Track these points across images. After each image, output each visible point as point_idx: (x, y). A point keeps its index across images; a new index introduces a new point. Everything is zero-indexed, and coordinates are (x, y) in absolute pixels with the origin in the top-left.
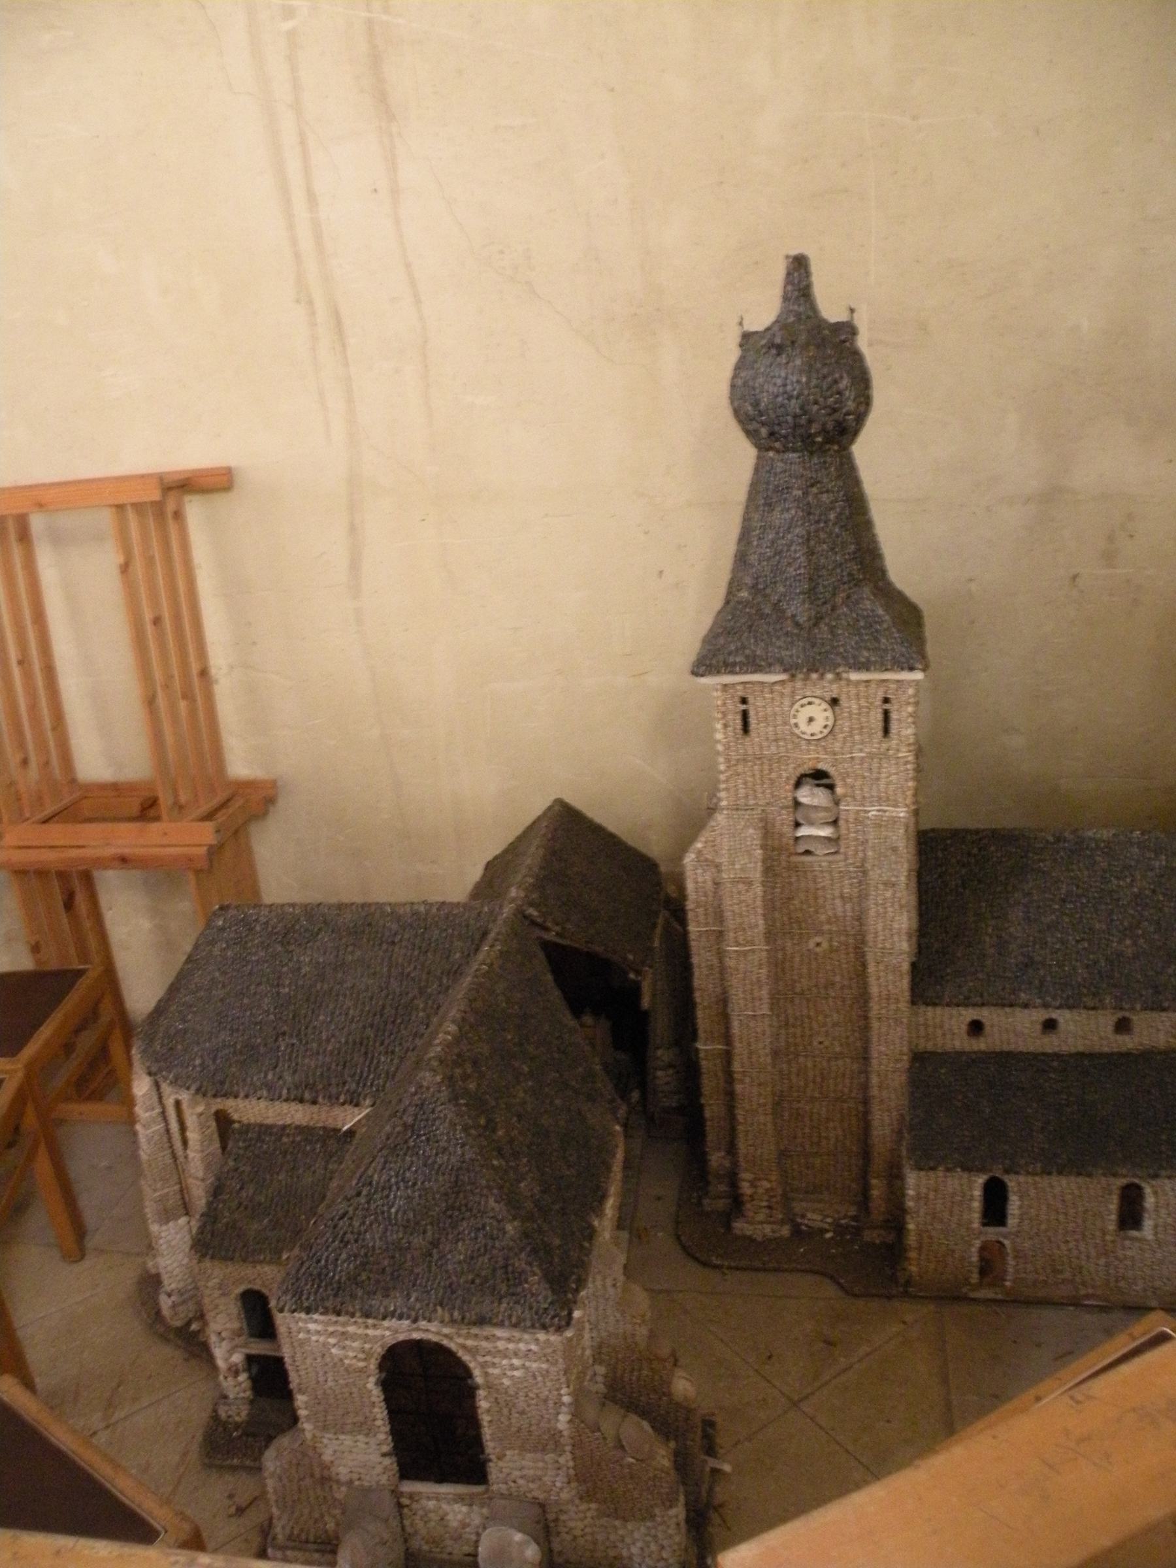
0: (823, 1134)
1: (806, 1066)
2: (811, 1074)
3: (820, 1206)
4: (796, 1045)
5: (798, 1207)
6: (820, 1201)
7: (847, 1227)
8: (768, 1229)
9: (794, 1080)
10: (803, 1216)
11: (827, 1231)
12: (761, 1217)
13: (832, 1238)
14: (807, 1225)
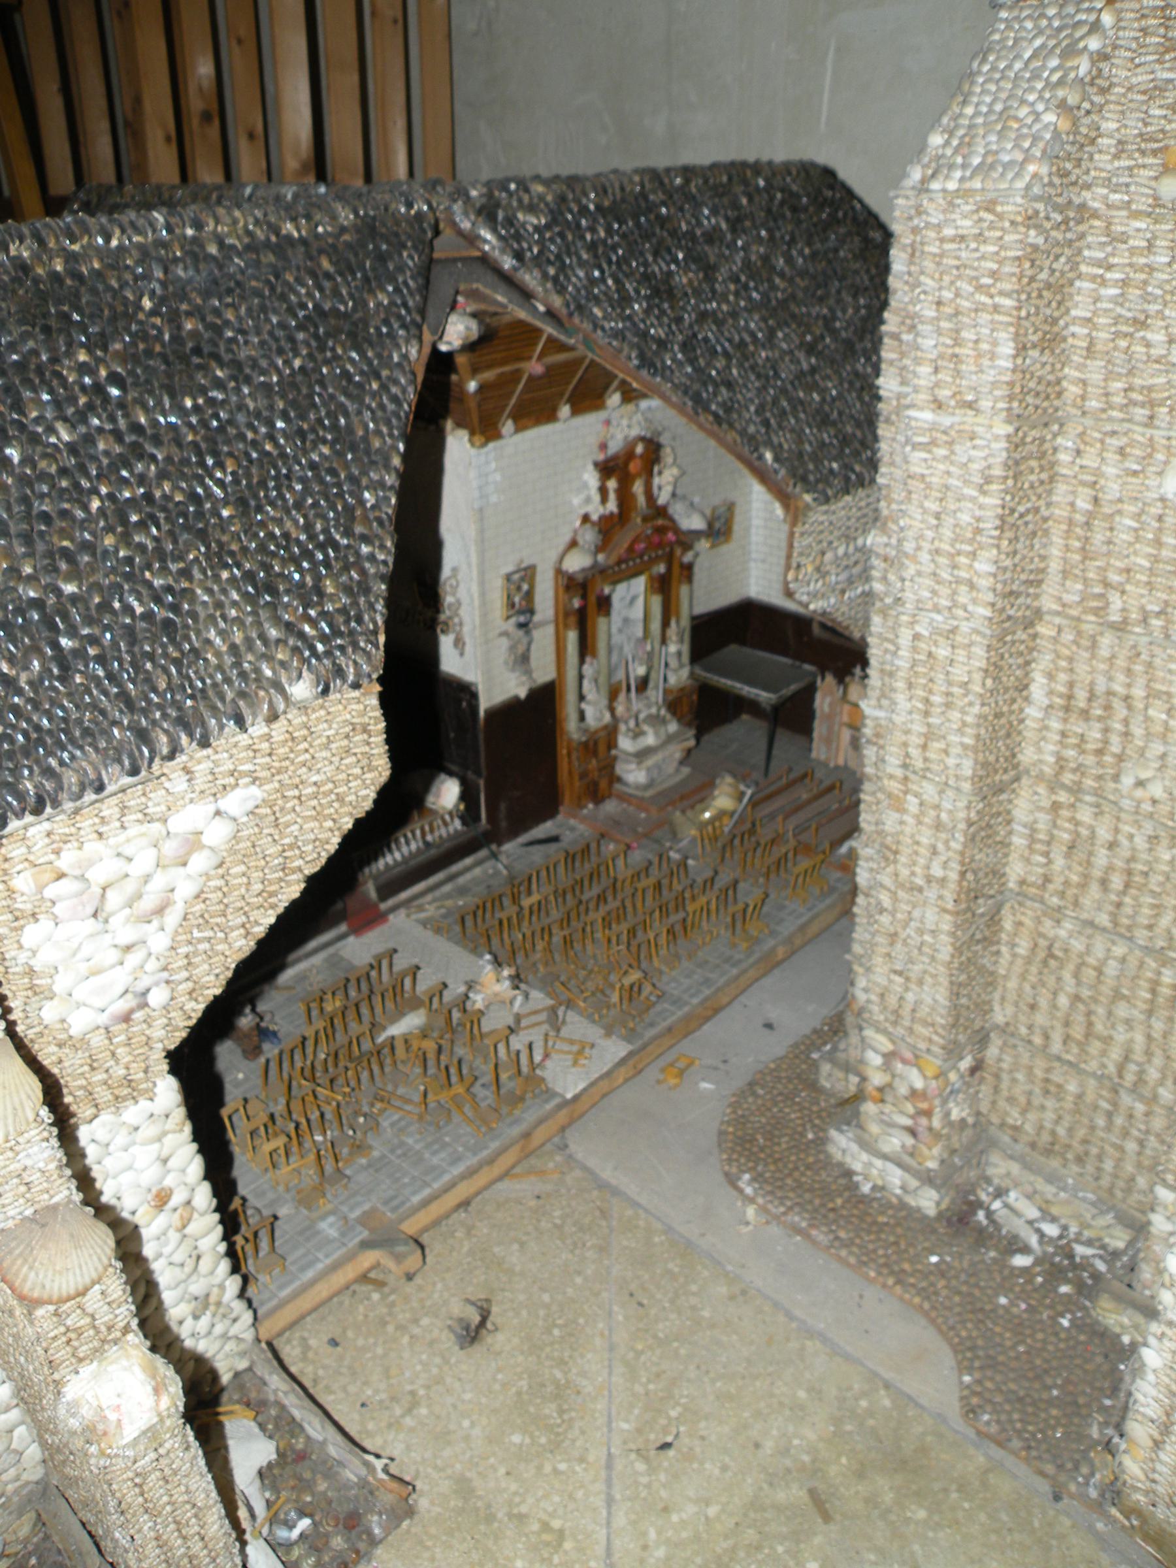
0: (1099, 1027)
1: (1093, 835)
2: (1101, 858)
3: (1049, 1190)
4: (1079, 769)
5: (999, 1167)
6: (1051, 1179)
7: (1086, 1265)
8: (895, 1178)
9: (1059, 862)
10: (1000, 1193)
11: (1025, 1250)
12: (895, 1142)
13: (1025, 1271)
14: (989, 1214)
